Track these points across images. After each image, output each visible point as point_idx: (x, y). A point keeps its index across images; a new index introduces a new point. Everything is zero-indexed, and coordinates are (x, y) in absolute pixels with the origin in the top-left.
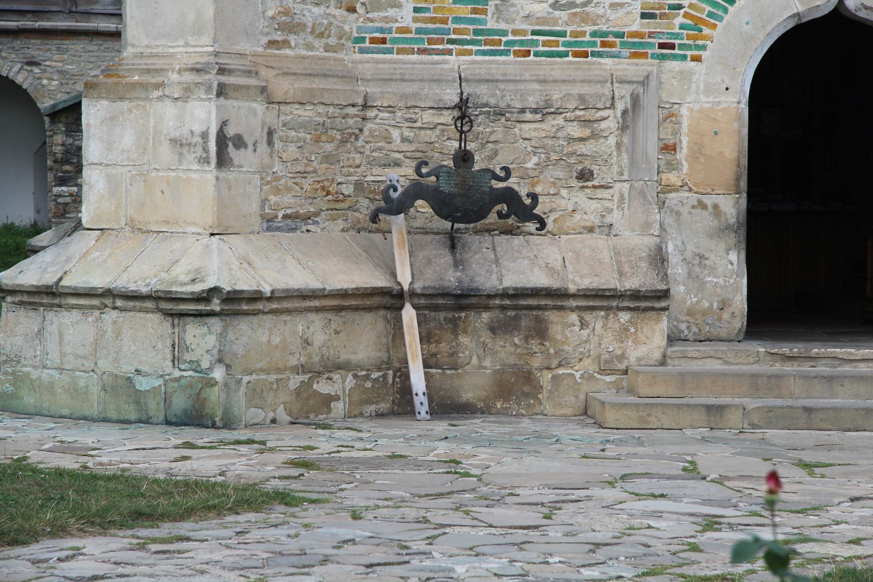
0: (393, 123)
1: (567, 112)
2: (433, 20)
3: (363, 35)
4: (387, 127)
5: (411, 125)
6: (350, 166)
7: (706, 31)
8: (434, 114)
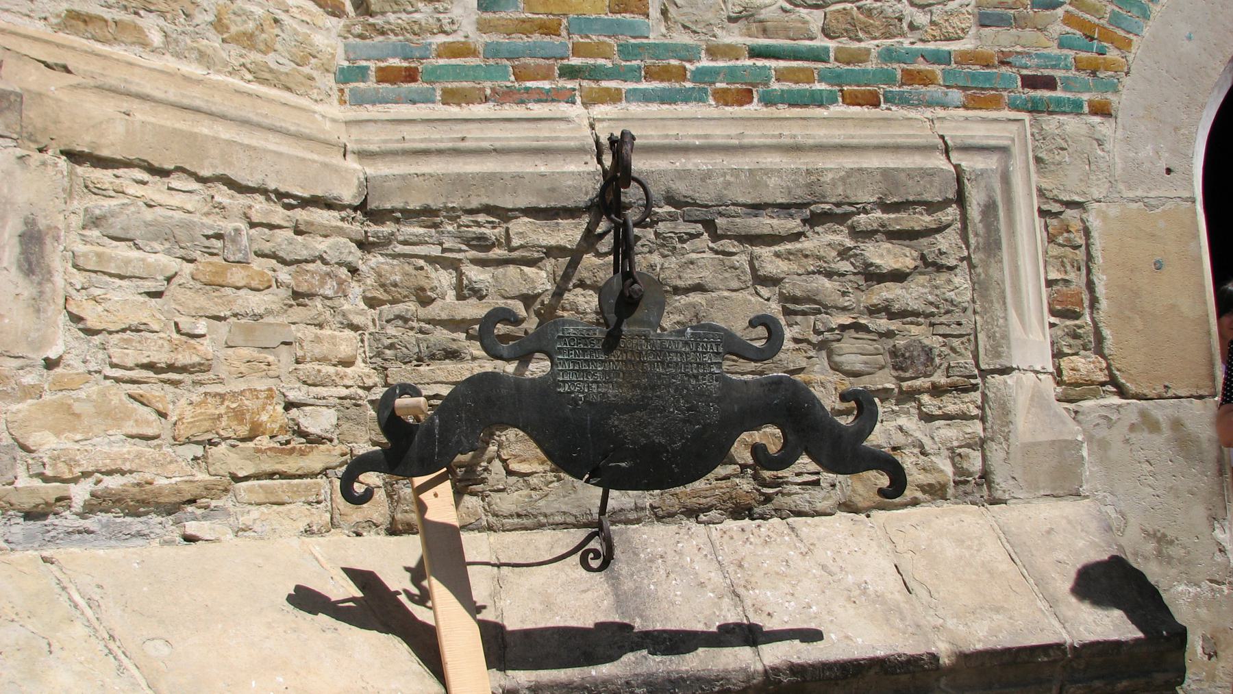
0: (435, 251)
2: (527, 26)
3: (364, 63)
7: (1113, 54)
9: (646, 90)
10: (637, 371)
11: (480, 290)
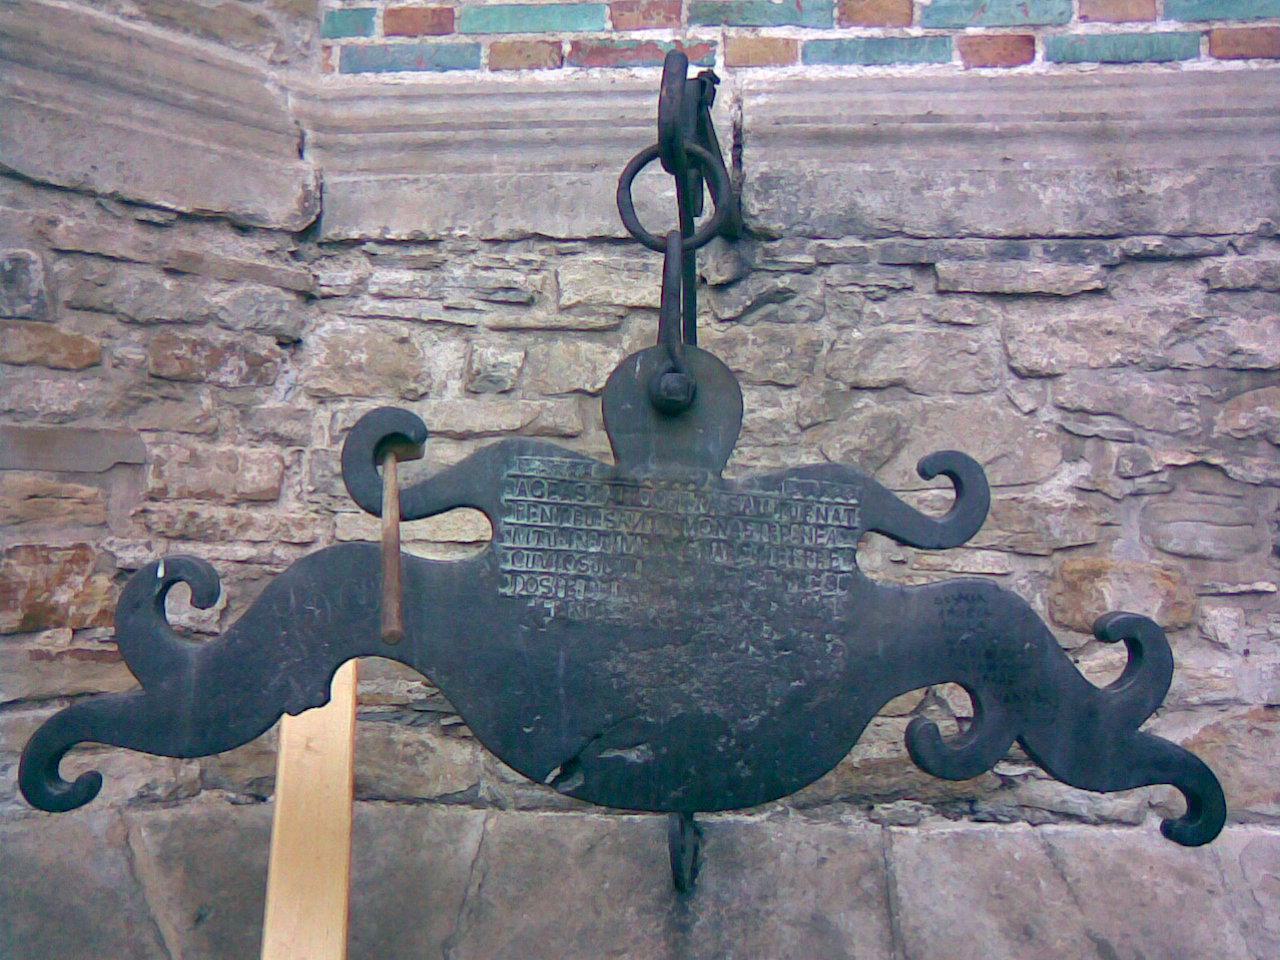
0: (432, 310)
1: (1220, 254)
4: (404, 330)
5: (508, 316)
6: (209, 495)
8: (611, 269)
9: (839, 41)
10: (672, 561)
11: (501, 380)
